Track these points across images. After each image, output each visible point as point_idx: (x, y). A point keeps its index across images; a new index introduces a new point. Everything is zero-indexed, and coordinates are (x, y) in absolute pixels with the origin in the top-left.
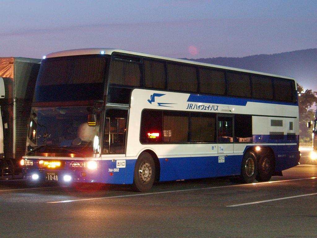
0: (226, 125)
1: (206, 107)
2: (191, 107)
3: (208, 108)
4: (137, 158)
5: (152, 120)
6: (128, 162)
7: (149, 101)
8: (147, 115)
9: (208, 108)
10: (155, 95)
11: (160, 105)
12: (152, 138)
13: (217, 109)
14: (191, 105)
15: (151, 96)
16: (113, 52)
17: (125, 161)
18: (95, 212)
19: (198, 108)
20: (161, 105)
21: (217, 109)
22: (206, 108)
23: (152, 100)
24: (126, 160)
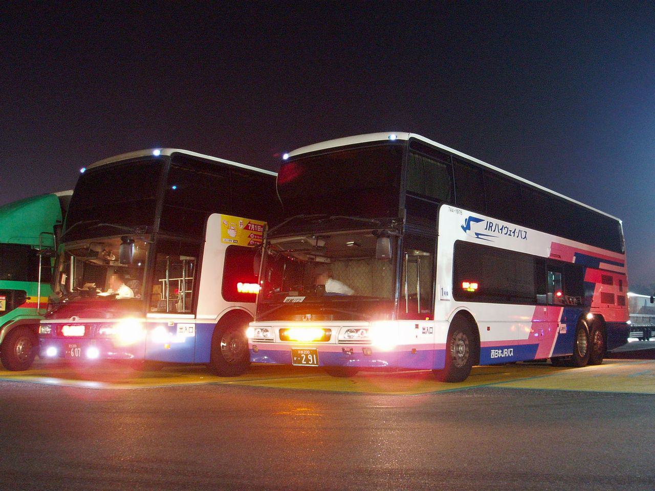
0: (286, 157)
1: (511, 231)
2: (491, 227)
3: (514, 232)
4: (216, 322)
5: (468, 257)
6: (199, 327)
7: (462, 227)
8: (461, 248)
9: (514, 232)
10: (471, 219)
11: (478, 237)
12: (470, 292)
13: (525, 237)
14: (491, 225)
15: (466, 219)
16: (411, 138)
17: (194, 326)
18: (390, 399)
19: (500, 231)
20: (479, 236)
21: (525, 237)
22: (511, 232)
23: (467, 228)
24: (196, 324)
